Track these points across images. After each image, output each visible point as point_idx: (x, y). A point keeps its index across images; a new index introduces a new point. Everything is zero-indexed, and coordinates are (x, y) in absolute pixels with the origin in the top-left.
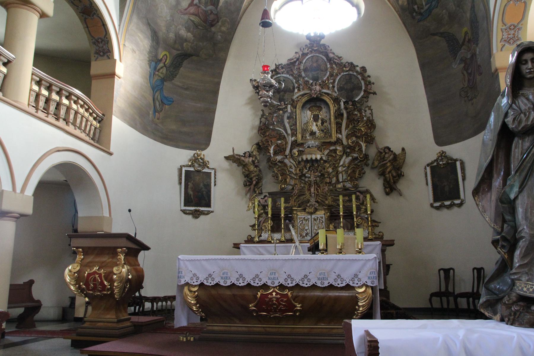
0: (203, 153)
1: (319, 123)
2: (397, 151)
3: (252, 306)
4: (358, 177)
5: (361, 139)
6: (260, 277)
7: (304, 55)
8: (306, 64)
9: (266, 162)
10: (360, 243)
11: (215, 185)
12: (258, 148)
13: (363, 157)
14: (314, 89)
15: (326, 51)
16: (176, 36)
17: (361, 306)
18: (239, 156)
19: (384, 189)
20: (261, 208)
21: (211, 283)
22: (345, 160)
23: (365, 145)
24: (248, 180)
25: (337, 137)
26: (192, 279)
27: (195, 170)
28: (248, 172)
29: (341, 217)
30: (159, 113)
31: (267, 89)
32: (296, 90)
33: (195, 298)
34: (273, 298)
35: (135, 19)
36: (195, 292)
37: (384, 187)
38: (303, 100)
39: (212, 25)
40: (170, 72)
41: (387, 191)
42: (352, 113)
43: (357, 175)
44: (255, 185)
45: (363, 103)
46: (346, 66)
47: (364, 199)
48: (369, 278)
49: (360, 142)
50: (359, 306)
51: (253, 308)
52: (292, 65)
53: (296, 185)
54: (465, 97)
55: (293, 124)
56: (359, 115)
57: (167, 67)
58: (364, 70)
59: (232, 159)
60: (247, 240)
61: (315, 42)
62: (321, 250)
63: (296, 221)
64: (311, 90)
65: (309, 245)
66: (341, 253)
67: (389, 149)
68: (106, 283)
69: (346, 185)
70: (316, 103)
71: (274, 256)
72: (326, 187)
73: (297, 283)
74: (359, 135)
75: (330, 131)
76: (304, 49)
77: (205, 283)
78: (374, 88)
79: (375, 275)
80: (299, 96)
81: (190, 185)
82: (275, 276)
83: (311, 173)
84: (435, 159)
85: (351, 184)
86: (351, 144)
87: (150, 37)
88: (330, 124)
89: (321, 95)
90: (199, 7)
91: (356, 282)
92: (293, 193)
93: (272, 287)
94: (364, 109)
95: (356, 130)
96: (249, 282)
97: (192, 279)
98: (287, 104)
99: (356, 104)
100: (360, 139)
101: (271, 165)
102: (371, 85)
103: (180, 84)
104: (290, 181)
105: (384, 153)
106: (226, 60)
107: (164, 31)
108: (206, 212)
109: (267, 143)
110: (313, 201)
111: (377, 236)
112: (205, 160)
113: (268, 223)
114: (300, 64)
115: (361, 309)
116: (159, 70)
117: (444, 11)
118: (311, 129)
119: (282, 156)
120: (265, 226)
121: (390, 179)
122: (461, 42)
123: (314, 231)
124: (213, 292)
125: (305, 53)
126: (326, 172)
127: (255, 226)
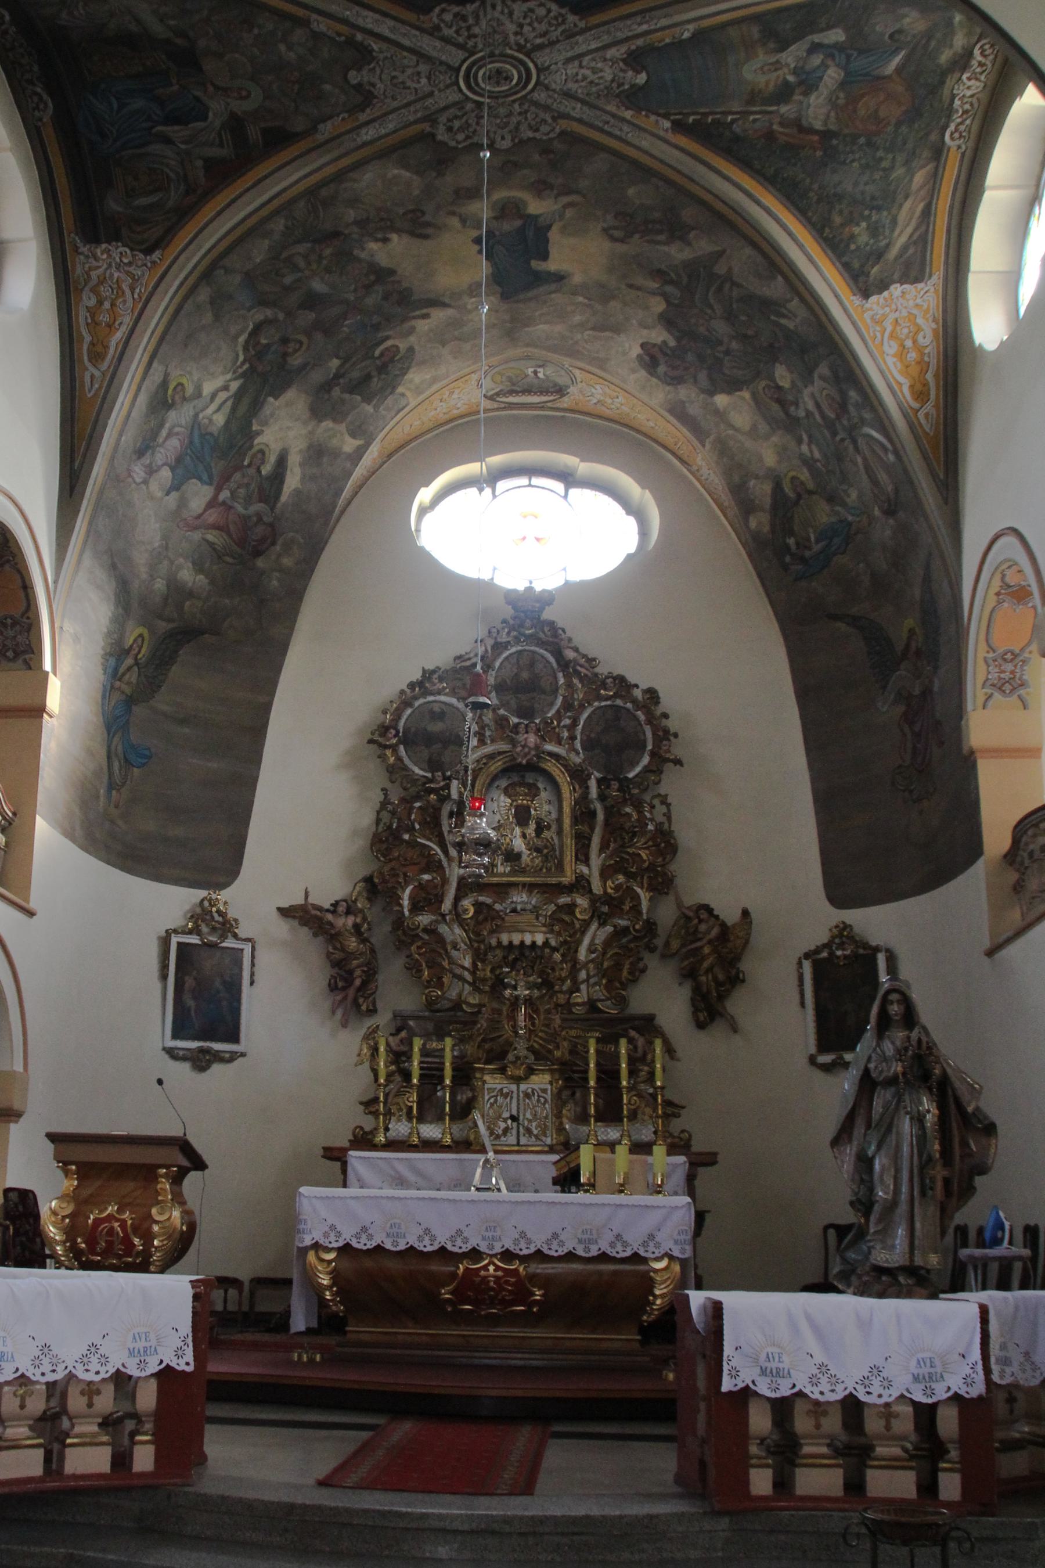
0: (224, 895)
2: (730, 915)
9: (389, 928)
11: (252, 983)
12: (369, 891)
16: (168, 586)
18: (320, 909)
22: (596, 935)
24: (341, 976)
26: (326, 1235)
30: (118, 790)
35: (88, 561)
36: (329, 1262)
38: (492, 768)
39: (257, 553)
41: (702, 1018)
42: (619, 811)
43: (625, 973)
44: (359, 989)
48: (676, 1242)
50: (655, 1297)
54: (904, 791)
56: (635, 816)
64: (514, 746)
66: (622, 1191)
67: (708, 909)
68: (136, 1241)
70: (523, 777)
74: (633, 870)
75: (557, 853)
76: (498, 632)
78: (677, 750)
80: (482, 758)
81: (189, 982)
83: (517, 975)
84: (826, 941)
87: (112, 597)
88: (560, 832)
90: (231, 507)
91: (651, 1248)
93: (488, 1255)
96: (443, 1244)
98: (449, 778)
99: (628, 787)
105: (696, 921)
106: (288, 645)
107: (144, 576)
108: (227, 1056)
110: (521, 1048)
111: (677, 1140)
112: (229, 916)
115: (658, 1302)
116: (123, 674)
117: (861, 565)
122: (899, 647)
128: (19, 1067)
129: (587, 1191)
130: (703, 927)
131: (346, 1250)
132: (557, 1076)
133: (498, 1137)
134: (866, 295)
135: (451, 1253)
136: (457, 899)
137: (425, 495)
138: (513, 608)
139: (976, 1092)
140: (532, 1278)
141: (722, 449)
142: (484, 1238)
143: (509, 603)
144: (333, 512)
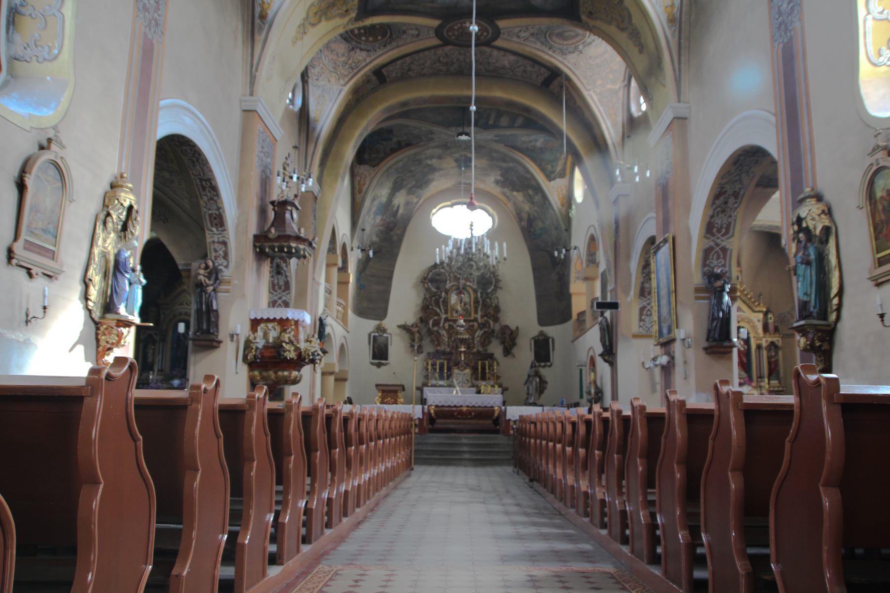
1: (462, 305)
2: (513, 327)
22: (479, 333)
32: (448, 282)
59: (404, 327)
78: (501, 284)
88: (470, 305)
128: (347, 369)
130: (506, 331)
131: (436, 406)
134: (550, 181)
136: (444, 323)
137: (434, 211)
139: (545, 377)
140: (472, 411)
141: (515, 204)
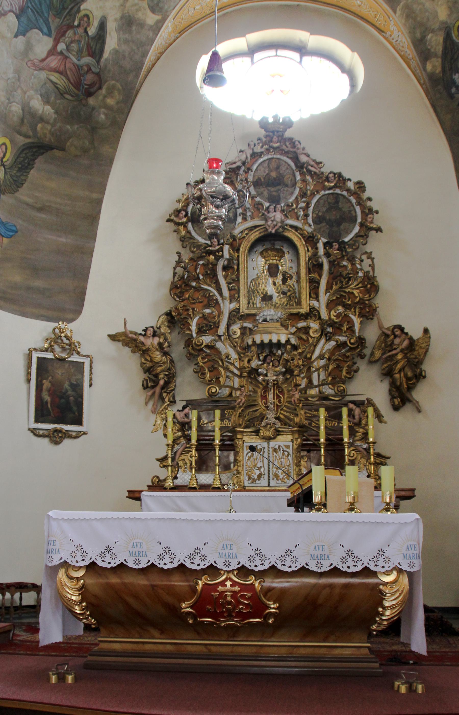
0: (71, 326)
3: (187, 606)
4: (345, 377)
5: (353, 310)
6: (113, 551)
7: (255, 156)
8: (259, 172)
9: (183, 346)
10: (388, 493)
11: (91, 385)
12: (169, 322)
13: (356, 342)
14: (272, 219)
15: (294, 150)
16: (23, 110)
17: (388, 607)
18: (136, 333)
19: (391, 400)
20: (177, 428)
21: (109, 563)
23: (359, 322)
25: (311, 305)
26: (73, 554)
27: (56, 357)
28: (151, 363)
29: (322, 446)
31: (218, 202)
32: (239, 219)
33: (79, 591)
34: (226, 592)
36: (78, 579)
37: (390, 397)
38: (252, 237)
39: (89, 94)
40: (11, 175)
41: (397, 403)
42: (338, 264)
43: (344, 373)
44: (163, 388)
45: (359, 246)
46: (330, 179)
47: (361, 416)
48: (405, 557)
49: (350, 315)
50: (384, 608)
51: (188, 610)
52: (233, 174)
53: (243, 388)
55: (234, 280)
56: (350, 267)
57: (6, 167)
58: (362, 187)
60: (151, 484)
61: (276, 133)
62: (316, 505)
63: (241, 451)
64: (266, 221)
65: (289, 495)
66: (351, 510)
67: (401, 329)
69: (324, 390)
70: (273, 244)
71: (228, 513)
72: (296, 392)
73: (273, 565)
74: (349, 302)
75: (297, 295)
76: (255, 145)
77: (100, 563)
78: (378, 221)
79: (415, 552)
80: (245, 230)
81: (46, 384)
82: (231, 551)
83: (267, 366)
85: (334, 390)
86: (335, 318)
88: (298, 281)
89: (284, 229)
90: (66, 57)
91: (381, 563)
92: (237, 402)
93: (225, 571)
94: (359, 257)
95: (344, 294)
96: (182, 561)
97: (74, 554)
99: (345, 247)
100: (350, 310)
101: (193, 352)
102: (373, 214)
103: (29, 200)
104: (225, 380)
105: (392, 337)
108: (74, 434)
109: (186, 313)
110: (271, 417)
112: (73, 339)
113: (189, 455)
114: (248, 172)
115: (388, 613)
118: (264, 290)
119: (213, 336)
120: (184, 460)
121: (401, 383)
123: (273, 471)
124: (114, 580)
125: (257, 153)
126: (297, 366)
127: (168, 459)
129: (319, 510)
132: (297, 436)
133: (254, 481)
135: (190, 569)
136: (228, 326)
138: (265, 130)
140: (268, 592)
142: (220, 556)
143: (262, 127)
144: (141, 68)
